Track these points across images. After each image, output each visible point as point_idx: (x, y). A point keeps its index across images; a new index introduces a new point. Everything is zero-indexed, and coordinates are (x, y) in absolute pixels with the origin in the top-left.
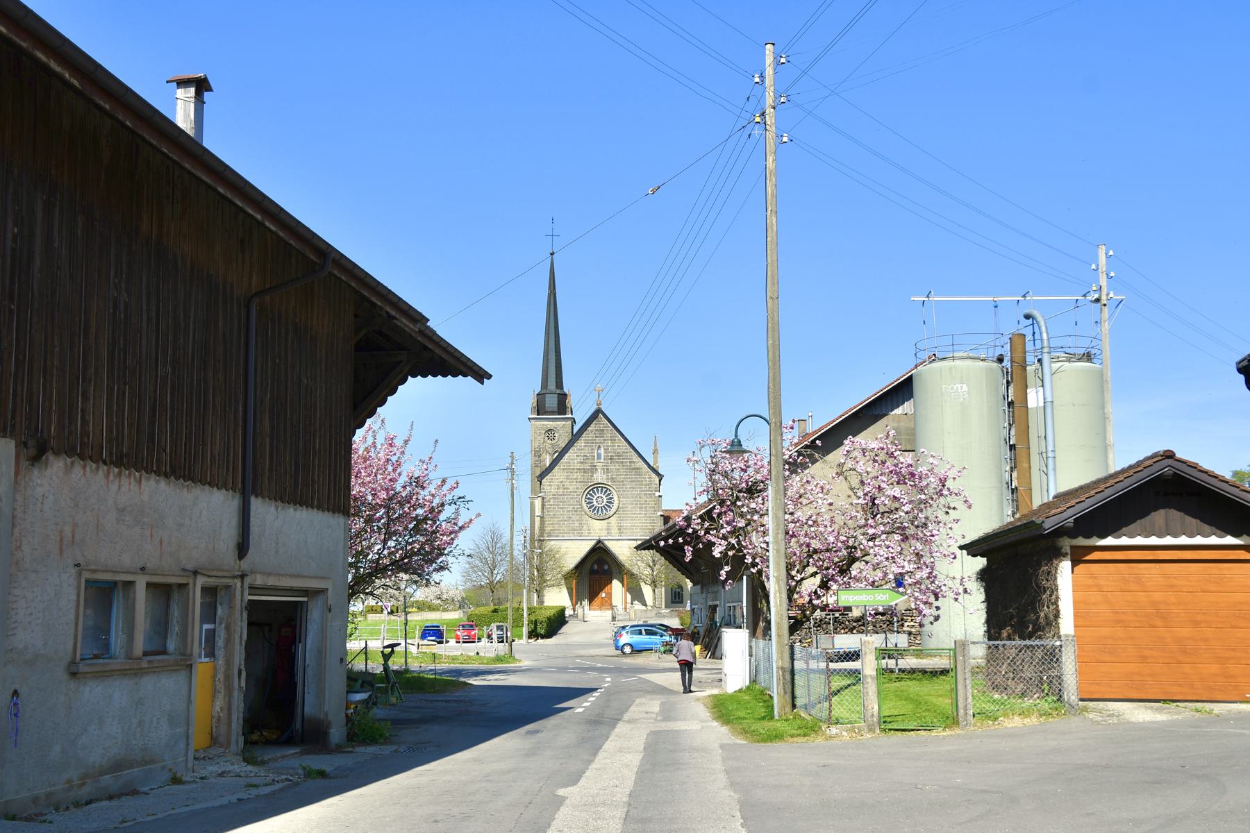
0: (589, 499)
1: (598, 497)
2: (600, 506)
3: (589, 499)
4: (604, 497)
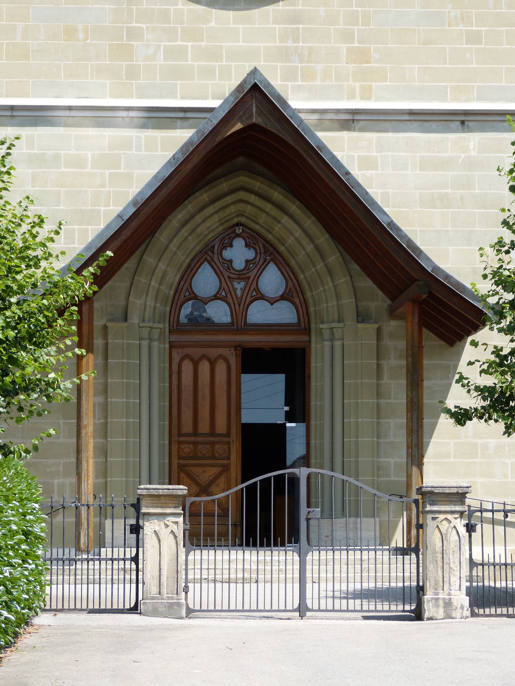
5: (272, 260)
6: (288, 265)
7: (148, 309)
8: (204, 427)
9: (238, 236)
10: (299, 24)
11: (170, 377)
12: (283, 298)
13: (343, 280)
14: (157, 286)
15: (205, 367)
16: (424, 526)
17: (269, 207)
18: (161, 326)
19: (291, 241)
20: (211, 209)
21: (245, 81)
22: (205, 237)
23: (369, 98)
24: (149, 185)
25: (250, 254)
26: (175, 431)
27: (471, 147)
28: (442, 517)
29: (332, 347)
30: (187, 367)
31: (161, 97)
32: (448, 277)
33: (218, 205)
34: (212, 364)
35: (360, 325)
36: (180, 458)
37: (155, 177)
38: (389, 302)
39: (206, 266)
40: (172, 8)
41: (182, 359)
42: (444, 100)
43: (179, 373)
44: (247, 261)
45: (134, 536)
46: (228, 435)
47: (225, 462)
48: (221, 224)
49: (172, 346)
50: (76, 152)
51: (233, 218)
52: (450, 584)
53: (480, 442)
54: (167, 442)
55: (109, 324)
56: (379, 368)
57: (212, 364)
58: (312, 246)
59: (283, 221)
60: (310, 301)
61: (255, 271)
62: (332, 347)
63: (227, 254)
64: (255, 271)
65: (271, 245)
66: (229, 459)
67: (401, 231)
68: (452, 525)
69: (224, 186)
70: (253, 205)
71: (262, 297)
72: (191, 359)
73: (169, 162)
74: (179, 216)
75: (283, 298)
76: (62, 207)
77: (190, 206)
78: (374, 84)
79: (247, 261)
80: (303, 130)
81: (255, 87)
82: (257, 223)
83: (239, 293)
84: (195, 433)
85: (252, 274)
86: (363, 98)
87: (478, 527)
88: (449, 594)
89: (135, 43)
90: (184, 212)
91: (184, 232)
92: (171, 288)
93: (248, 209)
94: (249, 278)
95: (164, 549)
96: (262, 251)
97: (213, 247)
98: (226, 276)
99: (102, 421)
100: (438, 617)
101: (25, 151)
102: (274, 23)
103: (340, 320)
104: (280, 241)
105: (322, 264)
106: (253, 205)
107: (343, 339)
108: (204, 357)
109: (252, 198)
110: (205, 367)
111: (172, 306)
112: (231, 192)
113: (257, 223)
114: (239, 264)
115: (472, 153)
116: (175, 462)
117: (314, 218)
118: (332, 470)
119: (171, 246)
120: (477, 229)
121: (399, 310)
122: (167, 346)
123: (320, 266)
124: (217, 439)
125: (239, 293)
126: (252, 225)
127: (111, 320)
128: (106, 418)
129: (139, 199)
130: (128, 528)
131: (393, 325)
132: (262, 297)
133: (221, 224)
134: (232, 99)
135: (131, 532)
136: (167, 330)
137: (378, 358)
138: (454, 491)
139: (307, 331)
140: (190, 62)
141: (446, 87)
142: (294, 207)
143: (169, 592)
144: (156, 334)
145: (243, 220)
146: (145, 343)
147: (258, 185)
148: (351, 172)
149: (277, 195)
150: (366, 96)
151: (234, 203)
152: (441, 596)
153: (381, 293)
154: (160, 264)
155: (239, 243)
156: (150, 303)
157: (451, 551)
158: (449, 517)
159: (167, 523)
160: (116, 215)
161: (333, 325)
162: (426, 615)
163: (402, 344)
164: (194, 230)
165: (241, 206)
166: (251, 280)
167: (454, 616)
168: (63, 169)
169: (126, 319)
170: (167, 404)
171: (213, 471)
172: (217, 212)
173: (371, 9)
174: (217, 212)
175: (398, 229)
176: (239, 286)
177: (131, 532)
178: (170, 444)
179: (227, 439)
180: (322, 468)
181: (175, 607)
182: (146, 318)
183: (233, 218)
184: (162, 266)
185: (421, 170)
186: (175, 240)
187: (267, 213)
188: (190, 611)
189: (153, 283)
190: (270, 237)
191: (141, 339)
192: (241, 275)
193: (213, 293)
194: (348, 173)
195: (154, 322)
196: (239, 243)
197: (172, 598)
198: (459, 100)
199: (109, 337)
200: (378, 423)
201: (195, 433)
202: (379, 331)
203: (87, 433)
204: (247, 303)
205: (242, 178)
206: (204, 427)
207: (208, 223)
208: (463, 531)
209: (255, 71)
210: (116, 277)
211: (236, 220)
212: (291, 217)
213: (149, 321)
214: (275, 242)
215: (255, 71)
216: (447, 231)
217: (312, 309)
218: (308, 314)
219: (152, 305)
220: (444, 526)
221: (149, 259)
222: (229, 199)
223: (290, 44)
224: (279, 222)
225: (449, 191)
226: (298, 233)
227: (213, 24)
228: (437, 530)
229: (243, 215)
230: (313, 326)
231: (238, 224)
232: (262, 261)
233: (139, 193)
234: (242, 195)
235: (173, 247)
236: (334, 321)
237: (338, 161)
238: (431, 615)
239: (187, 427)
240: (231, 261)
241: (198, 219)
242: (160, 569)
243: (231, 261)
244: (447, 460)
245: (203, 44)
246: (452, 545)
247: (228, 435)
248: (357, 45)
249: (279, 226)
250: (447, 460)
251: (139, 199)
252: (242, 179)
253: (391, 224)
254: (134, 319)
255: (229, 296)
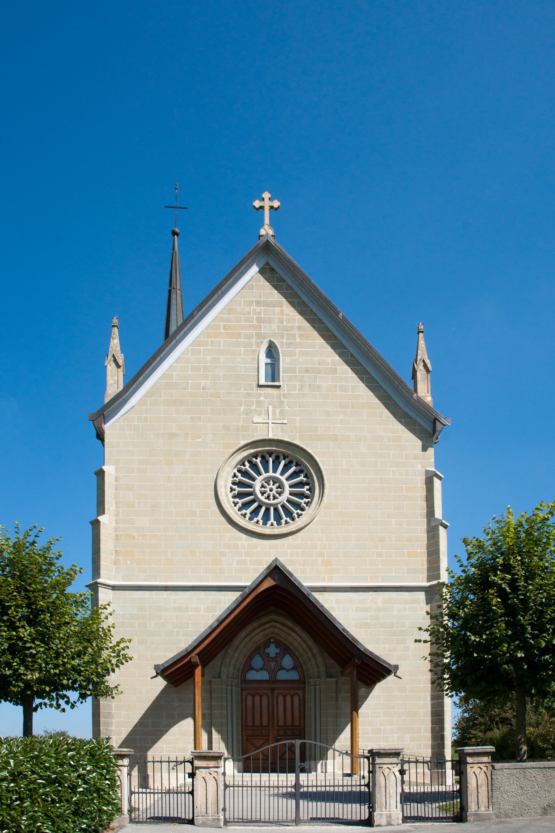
0: (254, 466)
1: (281, 486)
2: (262, 498)
3: (254, 466)
4: (287, 490)
5: (288, 653)
6: (295, 655)
7: (230, 673)
8: (257, 723)
9: (272, 642)
10: (299, 549)
11: (242, 702)
12: (292, 669)
13: (320, 660)
14: (234, 663)
15: (257, 698)
16: (374, 772)
17: (286, 629)
18: (237, 680)
19: (296, 644)
20: (259, 630)
21: (271, 564)
22: (256, 643)
23: (331, 581)
24: (225, 612)
25: (278, 651)
26: (244, 725)
27: (379, 602)
28: (385, 766)
29: (315, 689)
30: (249, 698)
31: (235, 581)
32: (371, 653)
33: (262, 628)
34: (261, 697)
35: (328, 679)
36: (247, 736)
37: (228, 608)
38: (341, 669)
39: (258, 655)
40: (240, 542)
41: (247, 695)
42: (367, 582)
43: (246, 701)
44: (276, 654)
45: (191, 780)
46: (268, 726)
47: (267, 737)
48: (264, 637)
49: (242, 689)
50: (196, 605)
51: (269, 635)
52: (390, 805)
53: (382, 728)
54: (240, 730)
55: (212, 680)
56: (337, 698)
57: (261, 697)
58: (306, 646)
59: (292, 635)
60: (305, 670)
61: (280, 657)
62: (315, 689)
63: (267, 650)
64: (280, 657)
65: (287, 646)
66: (268, 736)
67: (349, 632)
68: (392, 771)
69: (265, 620)
70: (278, 628)
71: (283, 669)
72: (251, 695)
73: (234, 601)
74: (244, 633)
75: (292, 669)
76: (190, 629)
77: (249, 629)
78: (334, 575)
79: (276, 654)
80: (300, 586)
81: (276, 567)
82: (280, 637)
83: (273, 667)
84: (253, 726)
85: (278, 659)
86: (329, 581)
87: (407, 772)
88: (390, 811)
89: (223, 558)
90: (246, 631)
91: (247, 640)
92: (241, 665)
93: (276, 630)
94: (277, 661)
95: (209, 788)
96: (283, 648)
97: (261, 647)
98: (267, 660)
99: (210, 720)
100: (383, 825)
101: (172, 605)
102: (287, 549)
103: (319, 677)
104: (291, 644)
105: (310, 653)
106: (278, 628)
107: (320, 685)
108: (257, 694)
109: (278, 625)
110: (257, 698)
111: (242, 673)
112: (268, 622)
113: (280, 637)
114: (272, 655)
115: (379, 605)
116: (244, 738)
117: (306, 633)
118: (315, 741)
119: (241, 646)
120: (382, 637)
121: (347, 671)
122: (240, 689)
123: (309, 654)
124: (264, 728)
125: (273, 667)
126: (278, 637)
127: (213, 678)
128: (212, 719)
129: (220, 619)
130: (187, 775)
131: (343, 678)
132: (283, 669)
133: (264, 637)
134: (265, 572)
135: (189, 777)
136: (240, 682)
137: (336, 693)
138: (394, 751)
139: (304, 682)
140: (248, 566)
141: (367, 576)
142: (297, 629)
143: (212, 812)
144: (234, 683)
145: (274, 635)
146: (229, 687)
147: (280, 619)
148: (324, 605)
149: (289, 623)
150: (330, 580)
151: (269, 627)
152: (384, 812)
153: (338, 665)
154: (235, 654)
155: (272, 646)
156: (231, 670)
157: (391, 786)
158: (390, 766)
159: (211, 772)
160: (208, 626)
161: (315, 679)
162: (376, 823)
163: (348, 687)
164: (251, 639)
165: (272, 629)
166: (278, 661)
167: (393, 824)
168: (190, 613)
169: (220, 677)
170: (240, 713)
171: (262, 741)
172: (261, 631)
173: (332, 543)
174: (261, 631)
175: (347, 632)
176: (273, 664)
177: (189, 777)
178: (242, 730)
179: (268, 728)
180: (311, 740)
181: (216, 821)
182: (229, 677)
183: (269, 635)
184: (236, 654)
185: (356, 612)
186: (242, 644)
187: (285, 632)
188: (226, 822)
189: (232, 662)
190: (286, 642)
191: (227, 686)
192: (273, 659)
193: (261, 667)
194: (322, 606)
195: (233, 679)
196: (272, 646)
197: (215, 816)
198: (373, 582)
199: (212, 685)
200: (336, 721)
201: (253, 726)
202: (337, 682)
203: (198, 725)
204: (276, 671)
205: (273, 616)
206: (257, 723)
207: (258, 637)
208: (398, 774)
209: (276, 559)
210: (215, 659)
211: (271, 636)
212: (296, 633)
213: (231, 678)
214: (289, 645)
215: (276, 559)
216: (368, 638)
217: (306, 673)
218: (304, 676)
219: (232, 671)
220: (386, 772)
221: (230, 652)
222: (267, 626)
223: (295, 558)
224: (290, 635)
225: (369, 621)
226: (299, 640)
227: (259, 549)
228: (382, 774)
229: (274, 633)
230: (306, 680)
231: (272, 638)
232: (283, 653)
233: (220, 616)
234: (273, 624)
235: (241, 646)
236: (316, 678)
237: (317, 601)
238: (378, 823)
239: (250, 723)
240: (269, 653)
241: (253, 634)
242: (207, 799)
243: (269, 653)
244: (368, 735)
245: (254, 558)
246: (391, 783)
247: (268, 726)
248: (325, 558)
249: (290, 637)
250: (368, 735)
251: (220, 619)
252: (273, 617)
253: (344, 629)
254: (224, 677)
255: (268, 668)
